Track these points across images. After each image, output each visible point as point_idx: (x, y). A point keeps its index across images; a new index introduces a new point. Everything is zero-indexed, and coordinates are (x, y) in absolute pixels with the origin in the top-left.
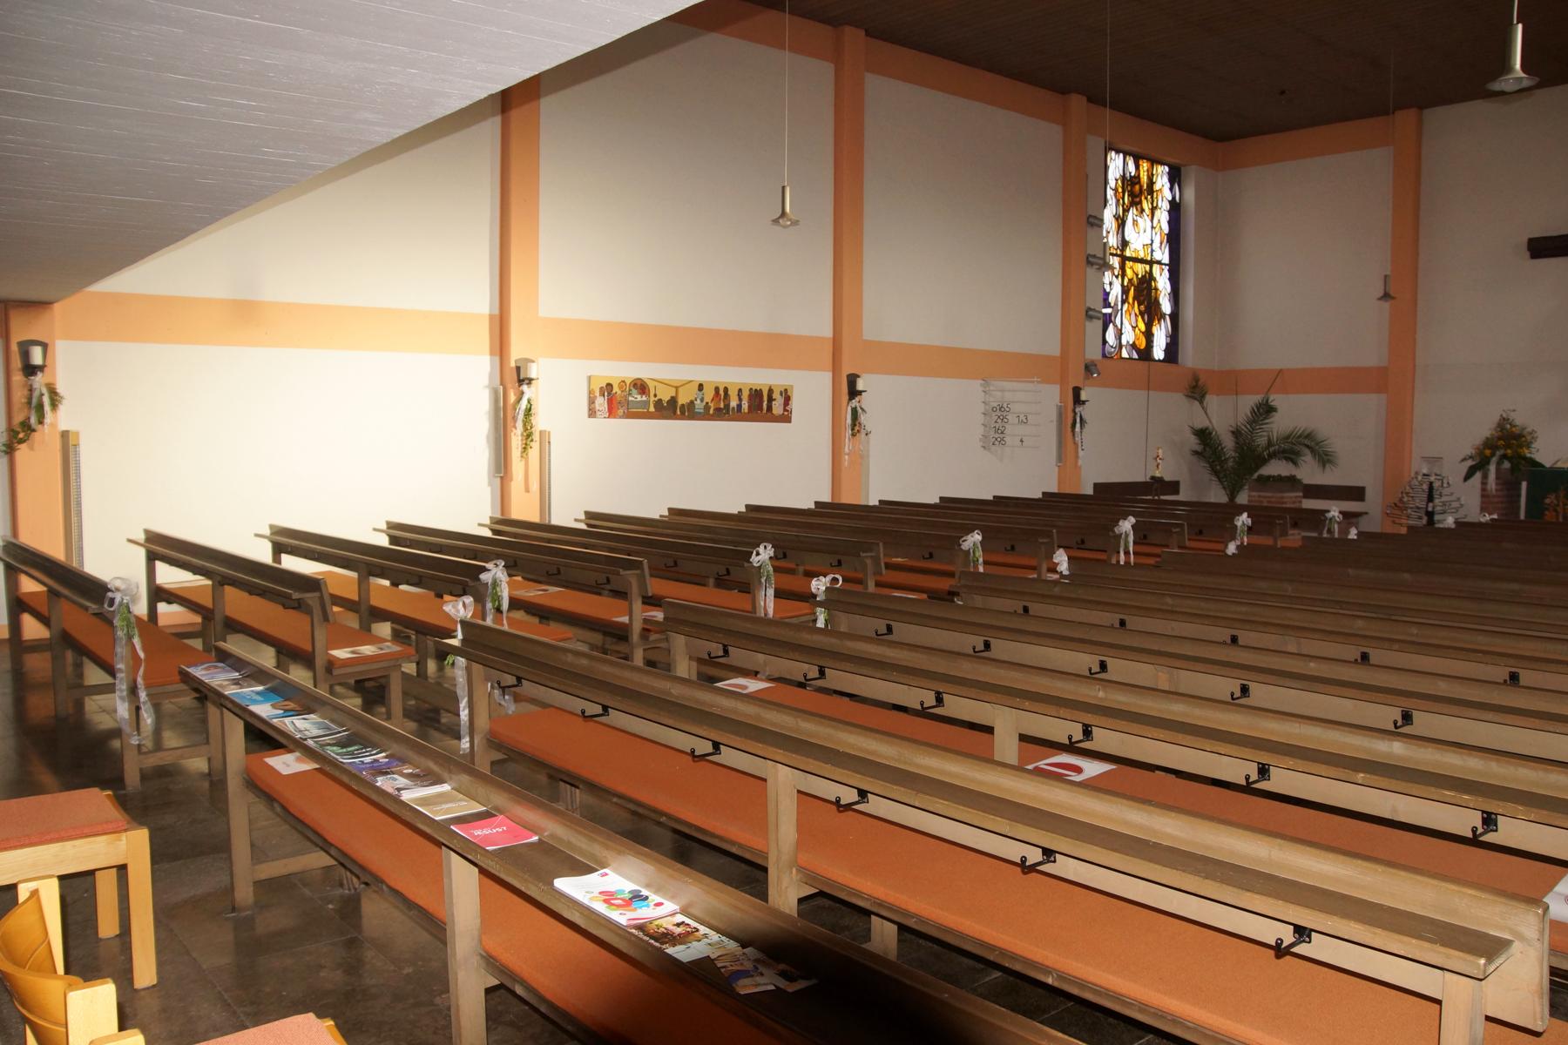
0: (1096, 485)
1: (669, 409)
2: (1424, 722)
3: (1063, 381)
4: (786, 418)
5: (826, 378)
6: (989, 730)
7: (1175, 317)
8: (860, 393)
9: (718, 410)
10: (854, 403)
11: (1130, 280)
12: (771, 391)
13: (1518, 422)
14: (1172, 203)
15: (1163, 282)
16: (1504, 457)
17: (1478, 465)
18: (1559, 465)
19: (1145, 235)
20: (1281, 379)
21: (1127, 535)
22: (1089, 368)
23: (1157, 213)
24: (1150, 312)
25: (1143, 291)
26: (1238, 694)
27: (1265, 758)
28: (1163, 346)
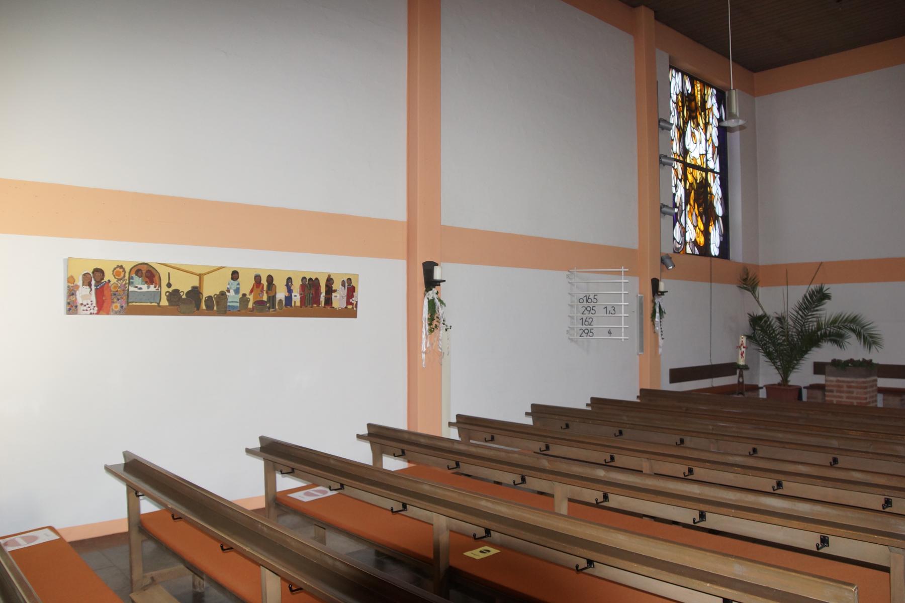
1: (190, 302)
2: (790, 487)
4: (350, 312)
5: (402, 264)
6: (552, 496)
7: (725, 218)
8: (437, 283)
9: (259, 303)
10: (432, 294)
11: (691, 184)
12: (330, 281)
15: (716, 189)
19: (700, 145)
22: (664, 261)
23: (710, 128)
24: (708, 214)
25: (700, 193)
26: (687, 473)
27: (703, 507)
28: (718, 244)
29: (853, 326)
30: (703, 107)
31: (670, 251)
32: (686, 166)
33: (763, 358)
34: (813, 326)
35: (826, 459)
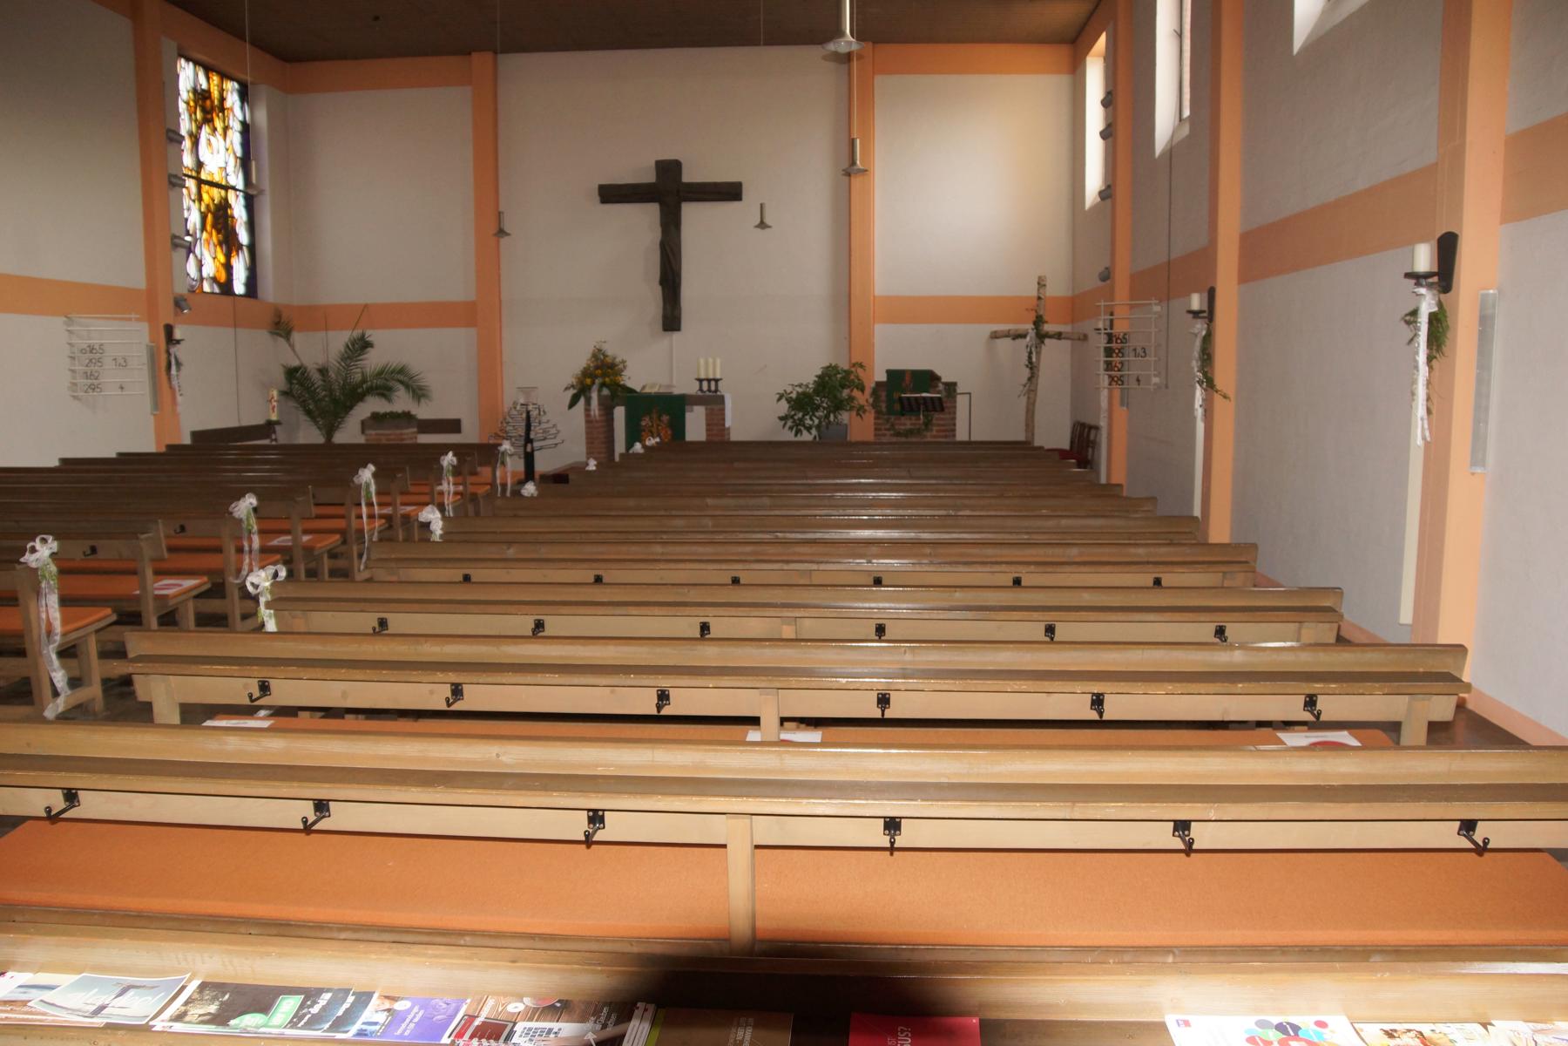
3: (151, 317)
7: (252, 248)
13: (609, 353)
14: (244, 124)
15: (239, 211)
16: (603, 385)
17: (581, 391)
18: (647, 390)
19: (218, 155)
20: (365, 313)
21: (368, 485)
22: (179, 303)
23: (230, 133)
24: (229, 243)
25: (220, 217)
29: (401, 377)
30: (222, 109)
31: (185, 292)
32: (200, 182)
33: (303, 417)
35: (525, 623)
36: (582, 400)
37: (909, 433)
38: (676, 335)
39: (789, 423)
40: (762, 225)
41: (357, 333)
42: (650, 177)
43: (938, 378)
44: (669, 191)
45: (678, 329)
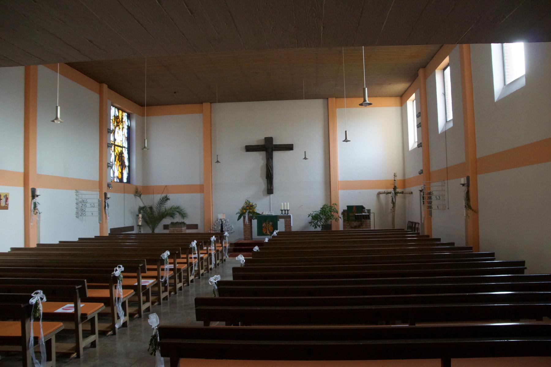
0: (111, 229)
5: (21, 189)
7: (129, 167)
10: (34, 201)
14: (128, 126)
15: (126, 155)
16: (249, 212)
17: (242, 215)
18: (264, 214)
19: (120, 137)
24: (122, 165)
25: (120, 156)
29: (178, 210)
30: (122, 122)
34: (163, 209)
36: (242, 218)
37: (355, 227)
38: (271, 195)
39: (313, 224)
40: (305, 158)
41: (164, 195)
42: (263, 143)
43: (364, 208)
44: (268, 148)
45: (272, 193)
